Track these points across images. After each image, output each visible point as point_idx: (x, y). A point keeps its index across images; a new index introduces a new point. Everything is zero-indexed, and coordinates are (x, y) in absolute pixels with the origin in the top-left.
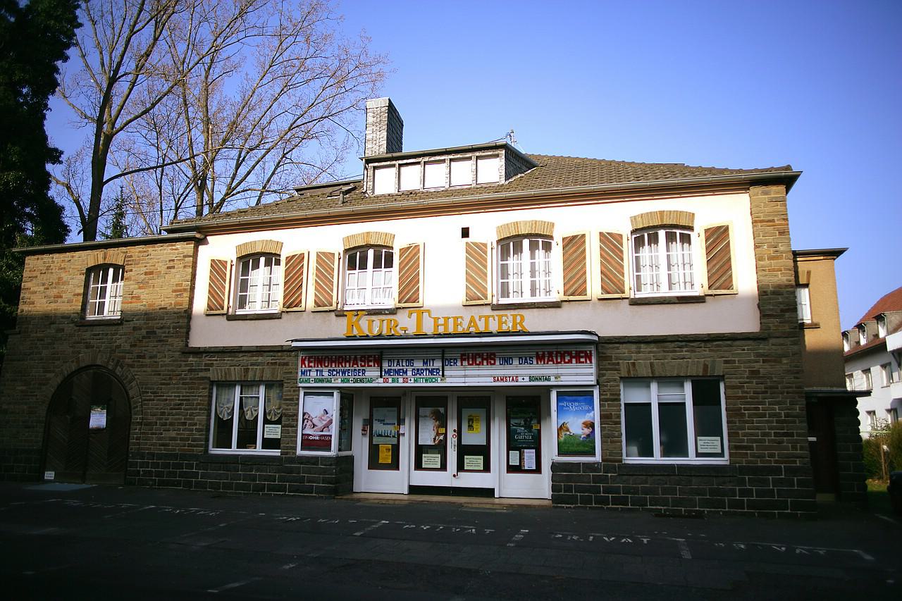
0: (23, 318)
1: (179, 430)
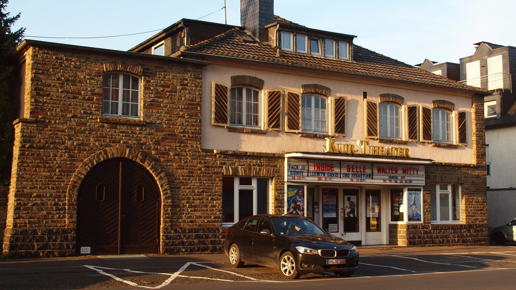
0: (478, 155)
1: (203, 210)
